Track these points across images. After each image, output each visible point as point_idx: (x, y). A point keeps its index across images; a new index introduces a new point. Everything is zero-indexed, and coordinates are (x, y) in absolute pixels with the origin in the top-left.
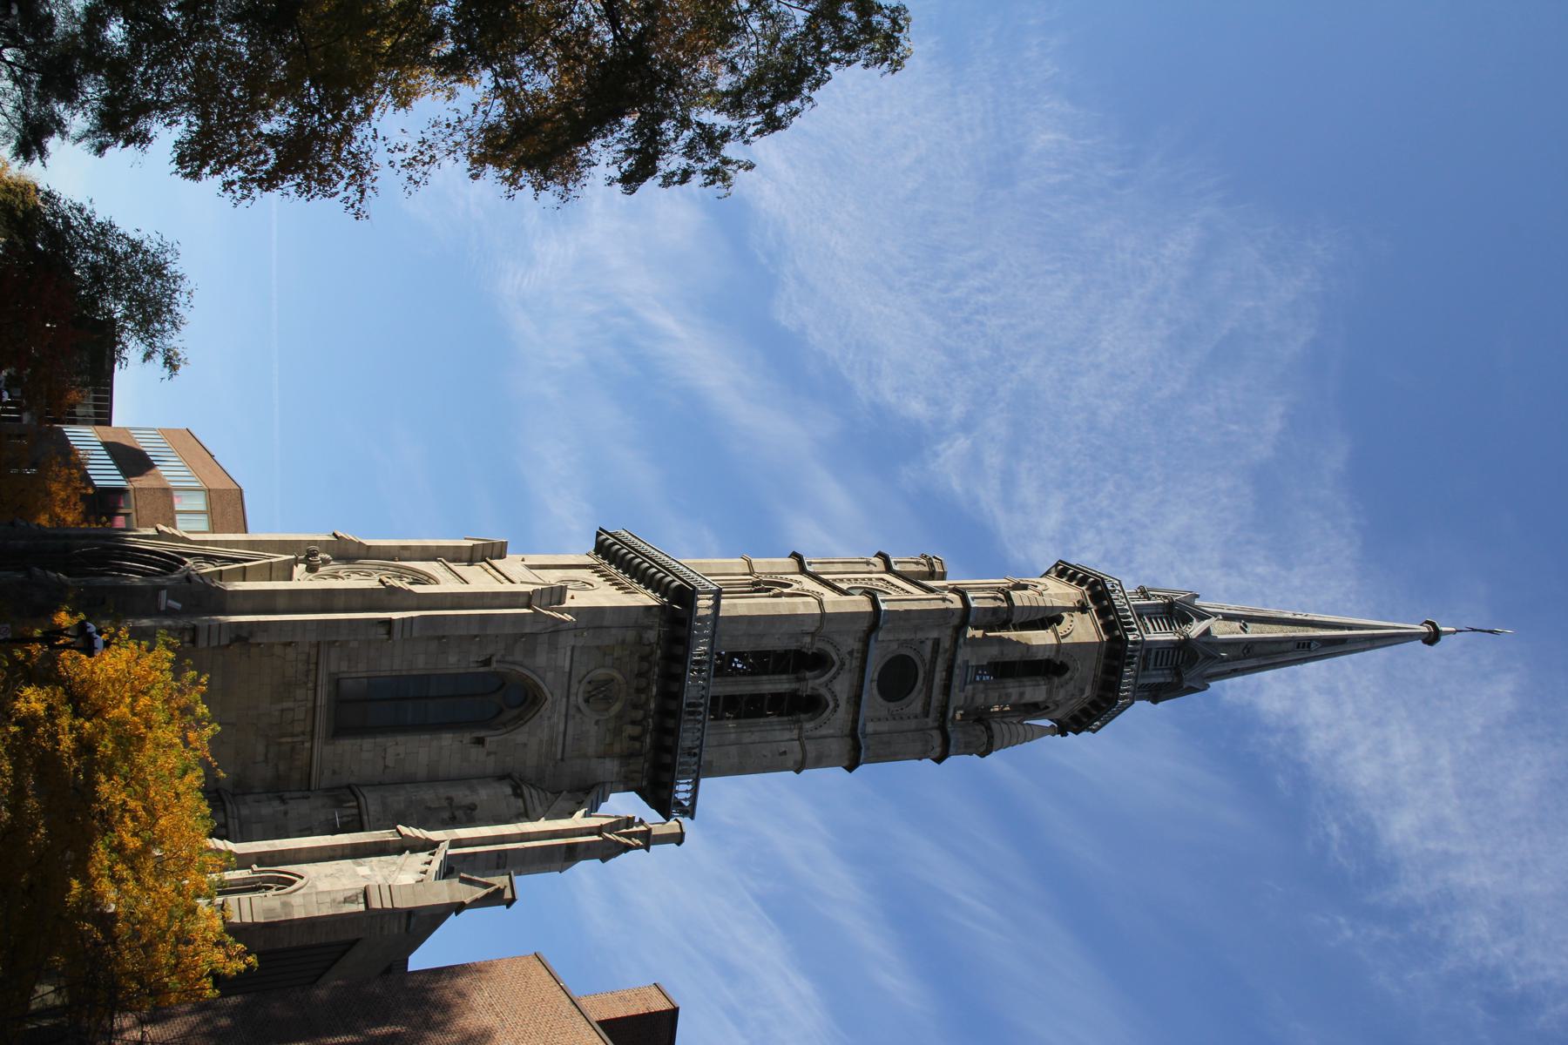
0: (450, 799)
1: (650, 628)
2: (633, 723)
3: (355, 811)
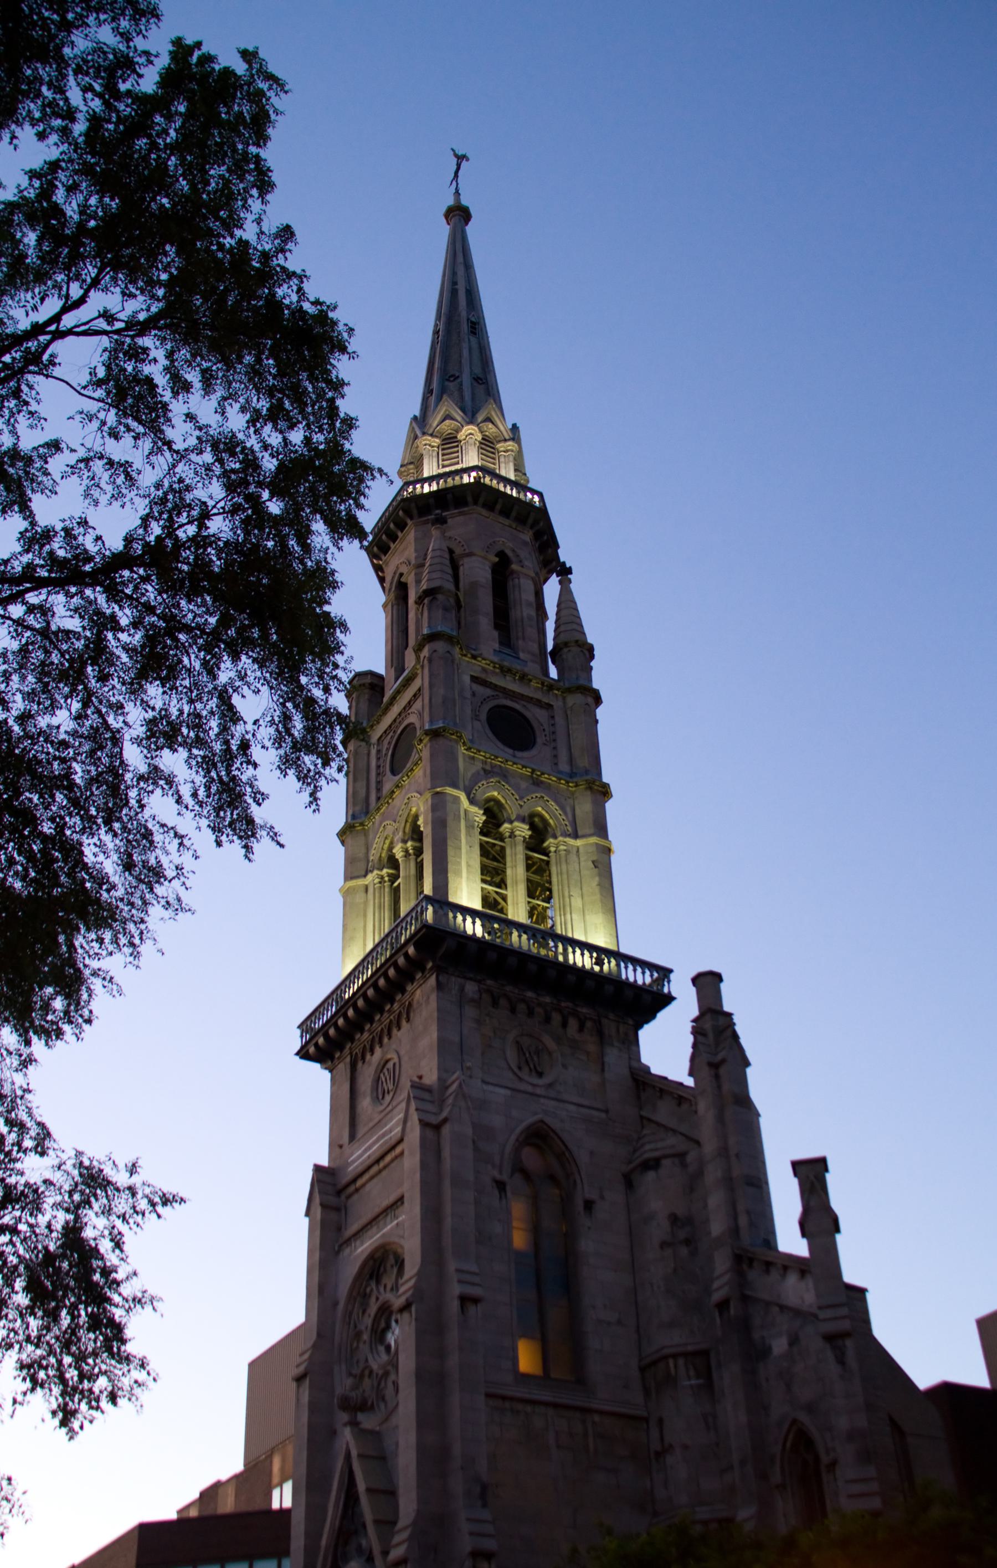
0: (663, 1245)
1: (462, 989)
2: (565, 1025)
3: (681, 1362)
